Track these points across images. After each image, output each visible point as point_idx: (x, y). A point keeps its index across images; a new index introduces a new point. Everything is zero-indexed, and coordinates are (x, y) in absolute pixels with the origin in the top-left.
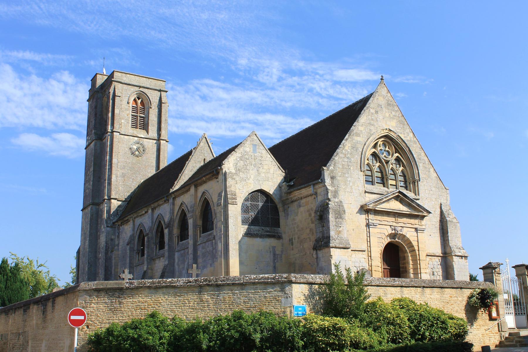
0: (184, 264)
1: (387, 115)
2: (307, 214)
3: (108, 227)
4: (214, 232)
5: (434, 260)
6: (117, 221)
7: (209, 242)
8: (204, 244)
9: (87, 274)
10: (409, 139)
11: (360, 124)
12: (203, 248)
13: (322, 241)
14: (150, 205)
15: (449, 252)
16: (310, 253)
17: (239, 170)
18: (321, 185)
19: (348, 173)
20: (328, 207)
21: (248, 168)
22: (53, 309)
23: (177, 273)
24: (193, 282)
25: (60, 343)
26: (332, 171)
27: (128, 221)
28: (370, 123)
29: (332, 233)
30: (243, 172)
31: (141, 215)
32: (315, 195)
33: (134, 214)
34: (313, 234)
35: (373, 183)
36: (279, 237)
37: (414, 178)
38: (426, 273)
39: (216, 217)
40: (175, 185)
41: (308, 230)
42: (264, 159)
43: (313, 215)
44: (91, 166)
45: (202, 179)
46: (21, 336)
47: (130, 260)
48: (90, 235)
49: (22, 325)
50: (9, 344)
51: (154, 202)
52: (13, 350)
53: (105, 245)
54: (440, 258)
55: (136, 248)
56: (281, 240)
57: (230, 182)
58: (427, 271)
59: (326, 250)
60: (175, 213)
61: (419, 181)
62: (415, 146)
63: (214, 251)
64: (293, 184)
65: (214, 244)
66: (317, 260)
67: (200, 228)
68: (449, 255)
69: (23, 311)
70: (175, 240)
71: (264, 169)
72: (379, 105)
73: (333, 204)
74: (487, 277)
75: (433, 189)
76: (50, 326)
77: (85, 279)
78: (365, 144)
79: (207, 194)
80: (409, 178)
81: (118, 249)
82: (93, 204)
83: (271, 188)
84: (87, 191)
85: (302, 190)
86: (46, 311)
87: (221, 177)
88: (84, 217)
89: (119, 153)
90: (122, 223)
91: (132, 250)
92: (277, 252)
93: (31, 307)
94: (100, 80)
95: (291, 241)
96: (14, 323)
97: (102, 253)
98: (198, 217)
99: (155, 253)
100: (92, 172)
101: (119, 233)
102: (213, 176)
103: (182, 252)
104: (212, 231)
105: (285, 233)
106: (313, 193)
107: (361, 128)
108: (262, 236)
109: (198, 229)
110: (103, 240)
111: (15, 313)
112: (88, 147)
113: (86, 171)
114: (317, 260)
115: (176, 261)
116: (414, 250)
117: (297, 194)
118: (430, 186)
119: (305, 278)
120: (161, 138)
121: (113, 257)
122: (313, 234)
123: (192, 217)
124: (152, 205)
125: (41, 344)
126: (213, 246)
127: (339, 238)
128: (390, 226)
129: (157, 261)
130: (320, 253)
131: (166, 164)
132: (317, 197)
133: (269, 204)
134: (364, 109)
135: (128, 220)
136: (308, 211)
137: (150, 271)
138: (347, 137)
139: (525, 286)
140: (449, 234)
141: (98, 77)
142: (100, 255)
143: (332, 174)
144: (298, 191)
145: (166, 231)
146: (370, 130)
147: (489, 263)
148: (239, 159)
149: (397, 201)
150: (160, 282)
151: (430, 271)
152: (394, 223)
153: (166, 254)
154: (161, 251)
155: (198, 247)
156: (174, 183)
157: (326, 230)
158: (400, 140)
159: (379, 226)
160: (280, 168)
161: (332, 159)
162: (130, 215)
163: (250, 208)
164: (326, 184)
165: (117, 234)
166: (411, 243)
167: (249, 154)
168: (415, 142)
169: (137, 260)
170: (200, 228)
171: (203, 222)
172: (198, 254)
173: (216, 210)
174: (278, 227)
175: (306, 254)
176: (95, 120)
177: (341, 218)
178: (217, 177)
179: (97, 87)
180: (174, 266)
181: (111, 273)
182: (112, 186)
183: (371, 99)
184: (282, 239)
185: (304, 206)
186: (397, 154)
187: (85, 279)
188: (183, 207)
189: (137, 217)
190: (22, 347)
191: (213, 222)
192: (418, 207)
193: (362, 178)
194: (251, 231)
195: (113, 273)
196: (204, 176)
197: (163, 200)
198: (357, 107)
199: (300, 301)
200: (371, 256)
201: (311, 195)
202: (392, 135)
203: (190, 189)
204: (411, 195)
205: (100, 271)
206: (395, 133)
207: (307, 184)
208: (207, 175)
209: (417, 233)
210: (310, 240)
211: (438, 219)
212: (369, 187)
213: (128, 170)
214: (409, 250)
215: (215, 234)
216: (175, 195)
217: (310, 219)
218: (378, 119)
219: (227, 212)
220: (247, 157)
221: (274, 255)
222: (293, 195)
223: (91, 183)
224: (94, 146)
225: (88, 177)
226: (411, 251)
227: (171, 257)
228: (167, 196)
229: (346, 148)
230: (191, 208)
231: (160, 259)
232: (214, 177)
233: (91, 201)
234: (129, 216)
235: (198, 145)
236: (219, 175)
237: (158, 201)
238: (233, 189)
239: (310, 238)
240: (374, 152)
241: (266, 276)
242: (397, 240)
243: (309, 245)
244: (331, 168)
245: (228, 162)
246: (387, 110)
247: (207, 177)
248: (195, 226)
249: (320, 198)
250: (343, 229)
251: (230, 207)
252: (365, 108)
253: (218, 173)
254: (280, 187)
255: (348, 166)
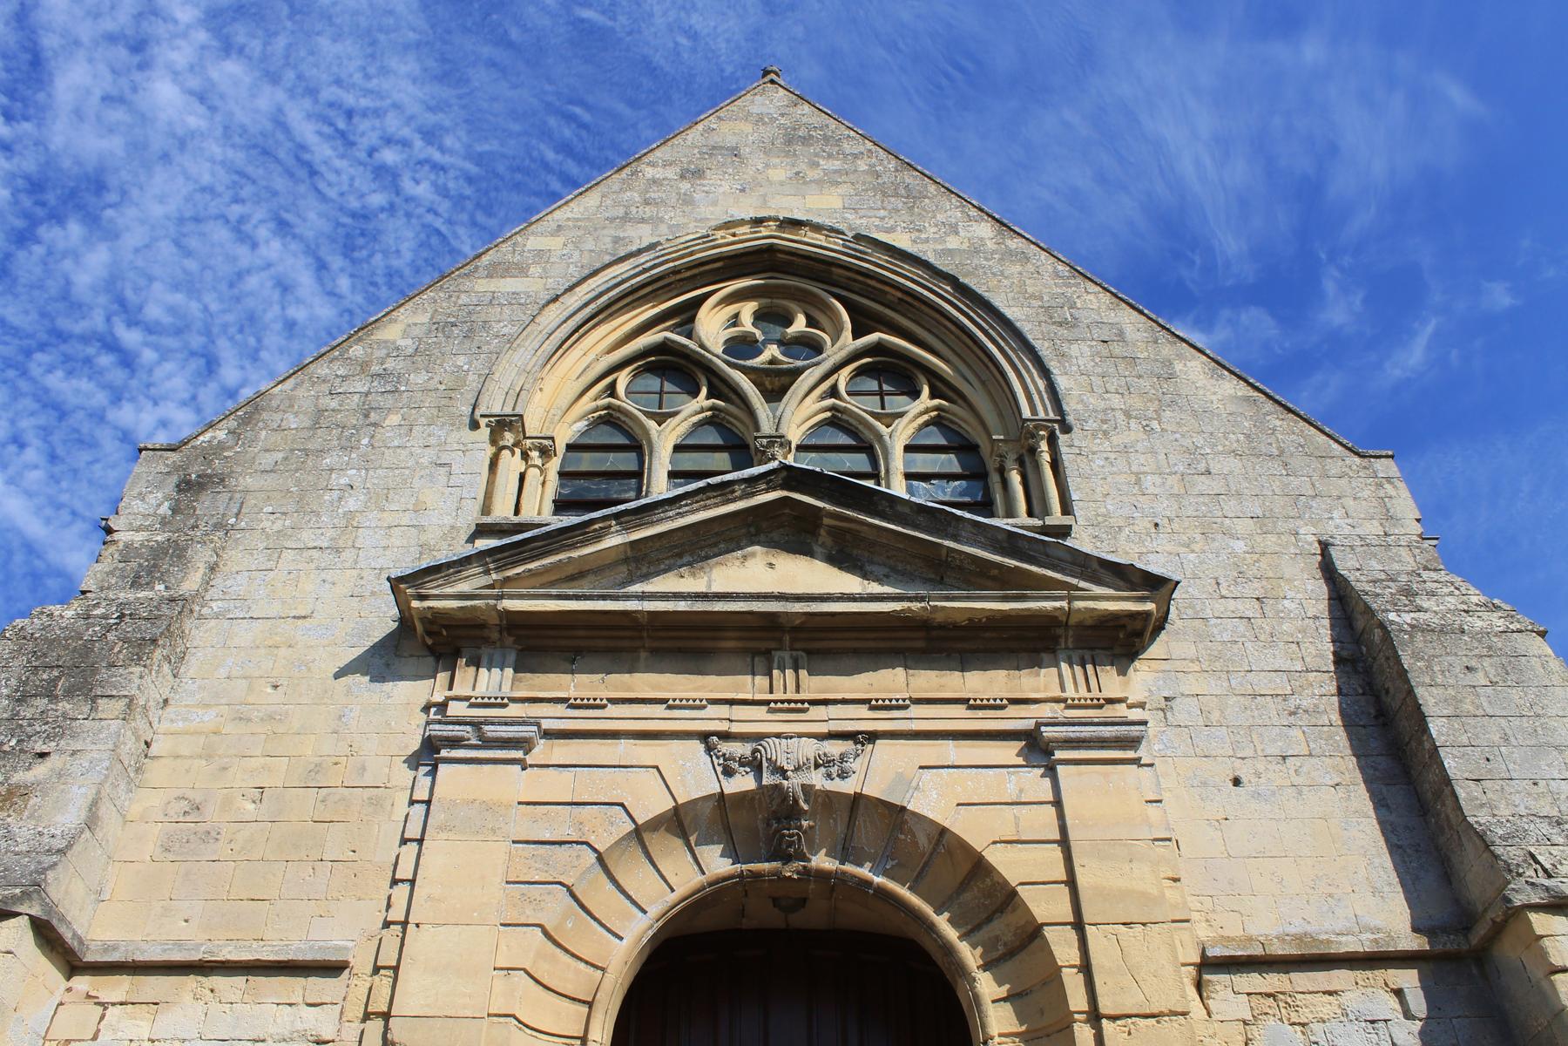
5: (1326, 1006)
54: (1408, 979)
116: (1034, 933)
128: (704, 737)
140: (1435, 727)
149: (809, 553)
158: (882, 258)
159: (543, 751)
166: (979, 867)
192: (1013, 563)
206: (832, 230)
209: (1051, 771)
211: (1321, 647)
214: (989, 946)
226: (1011, 954)
242: (822, 861)
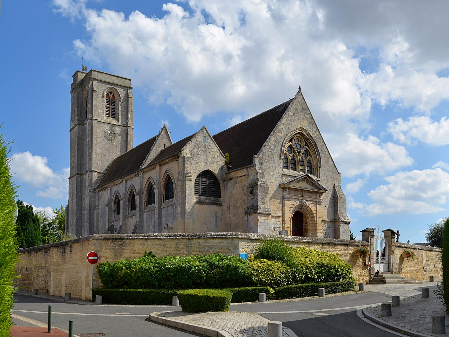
0: (151, 221)
1: (302, 117)
2: (241, 189)
3: (90, 192)
4: (174, 199)
6: (97, 188)
7: (171, 207)
8: (167, 208)
9: (75, 226)
10: (316, 136)
11: (282, 123)
12: (166, 211)
13: (252, 209)
14: (124, 177)
15: (337, 219)
16: (242, 217)
17: (193, 155)
18: (252, 169)
19: (272, 160)
20: (257, 185)
21: (200, 153)
22: (70, 252)
23: (145, 228)
24: (172, 237)
25: (78, 275)
26: (261, 159)
27: (106, 188)
28: (289, 123)
29: (259, 204)
30: (196, 157)
31: (116, 185)
32: (248, 175)
33: (111, 183)
34: (245, 203)
35: (289, 168)
36: (220, 205)
37: (317, 165)
38: (320, 233)
39: (176, 189)
40: (143, 163)
41: (241, 201)
42: (211, 148)
43: (245, 190)
44: (76, 145)
45: (166, 161)
46: (44, 269)
47: (109, 217)
48: (76, 197)
49: (44, 261)
50: (33, 274)
51: (128, 176)
52: (37, 278)
53: (89, 205)
55: (113, 208)
56: (222, 207)
57: (187, 164)
58: (322, 231)
59: (255, 215)
60: (144, 185)
61: (321, 167)
62: (319, 141)
63: (174, 213)
64: (231, 166)
65: (174, 208)
66: (247, 222)
67: (163, 196)
68: (337, 220)
69: (44, 252)
70: (144, 204)
71: (211, 155)
72: (296, 109)
73: (261, 183)
74: (365, 237)
75: (330, 173)
76: (69, 263)
77: (74, 230)
78: (285, 139)
79: (169, 171)
80: (313, 164)
81: (99, 209)
82: (78, 174)
83: (215, 168)
84: (73, 164)
85: (238, 171)
86: (64, 252)
87: (180, 160)
88: (71, 184)
89: (97, 136)
90: (101, 189)
91: (110, 210)
92: (219, 215)
93: (51, 250)
94: (80, 77)
95: (228, 207)
96: (37, 260)
97: (86, 211)
98: (162, 188)
99: (128, 213)
100: (77, 150)
101: (99, 197)
102: (174, 159)
103: (150, 213)
104: (173, 199)
105: (224, 202)
106: (247, 174)
107: (282, 127)
108: (208, 204)
109: (162, 197)
110: (86, 201)
111: (37, 253)
112: (72, 130)
113: (71, 149)
114: (247, 222)
115: (145, 219)
117: (234, 174)
118: (328, 171)
119: (247, 235)
120: (128, 125)
121: (95, 214)
122: (245, 203)
123: (158, 188)
124: (126, 178)
125: (61, 274)
126: (174, 210)
127: (263, 207)
129: (130, 219)
130: (250, 218)
131: (135, 146)
132: (249, 177)
133: (214, 181)
134: (285, 112)
135: (106, 187)
136: (242, 187)
137: (124, 226)
138: (272, 133)
139: (389, 244)
140: (338, 206)
141: (78, 74)
142: (85, 212)
143: (260, 161)
144: (235, 172)
145: (137, 198)
146: (289, 128)
147: (367, 228)
148: (193, 147)
150: (149, 236)
151: (323, 231)
152: (301, 197)
153: (138, 214)
154: (132, 211)
155: (162, 210)
156: (143, 162)
157: (255, 201)
160: (222, 154)
161: (261, 150)
162: (108, 184)
163: (200, 183)
164: (256, 168)
165: (97, 198)
167: (201, 143)
168: (319, 138)
169: (114, 217)
170: (163, 196)
171: (165, 191)
172: (162, 215)
173: (177, 184)
174: (219, 198)
175: (239, 218)
176: (77, 109)
177: (266, 193)
178: (177, 159)
179: (78, 82)
180: (143, 222)
181: (94, 226)
182: (93, 161)
183: (291, 104)
184: (222, 206)
185: (239, 183)
186: (307, 147)
187: (74, 230)
188: (150, 180)
189: (113, 185)
190: (45, 277)
191: (173, 193)
193: (282, 164)
194: (201, 200)
195: (95, 226)
196: (168, 158)
197: (135, 174)
198: (280, 110)
199: (243, 251)
200: (284, 220)
201: (245, 175)
202: (304, 133)
203: (156, 167)
204: (314, 177)
205: (85, 224)
207: (243, 168)
208: (170, 157)
210: (242, 207)
212: (286, 171)
213: (104, 149)
214: (310, 217)
215: (175, 201)
216: (144, 171)
217: (243, 193)
218: (295, 120)
219: (185, 186)
220: (199, 145)
221: (217, 217)
222: (231, 175)
223: (77, 158)
224: (77, 130)
225: (73, 153)
227: (141, 216)
228: (138, 172)
229: (271, 141)
230: (157, 181)
231: (132, 217)
232: (175, 159)
233: (76, 172)
234: (107, 185)
235: (160, 133)
236: (179, 159)
237: (130, 174)
238: (189, 169)
239: (242, 206)
240: (290, 145)
241: (222, 233)
243: (242, 211)
244: (260, 156)
245: (186, 148)
246: (301, 113)
247: (170, 159)
248: (160, 194)
249: (251, 178)
250: (267, 201)
251: (187, 183)
252: (286, 111)
253: (178, 157)
254: (222, 168)
255: (272, 155)
